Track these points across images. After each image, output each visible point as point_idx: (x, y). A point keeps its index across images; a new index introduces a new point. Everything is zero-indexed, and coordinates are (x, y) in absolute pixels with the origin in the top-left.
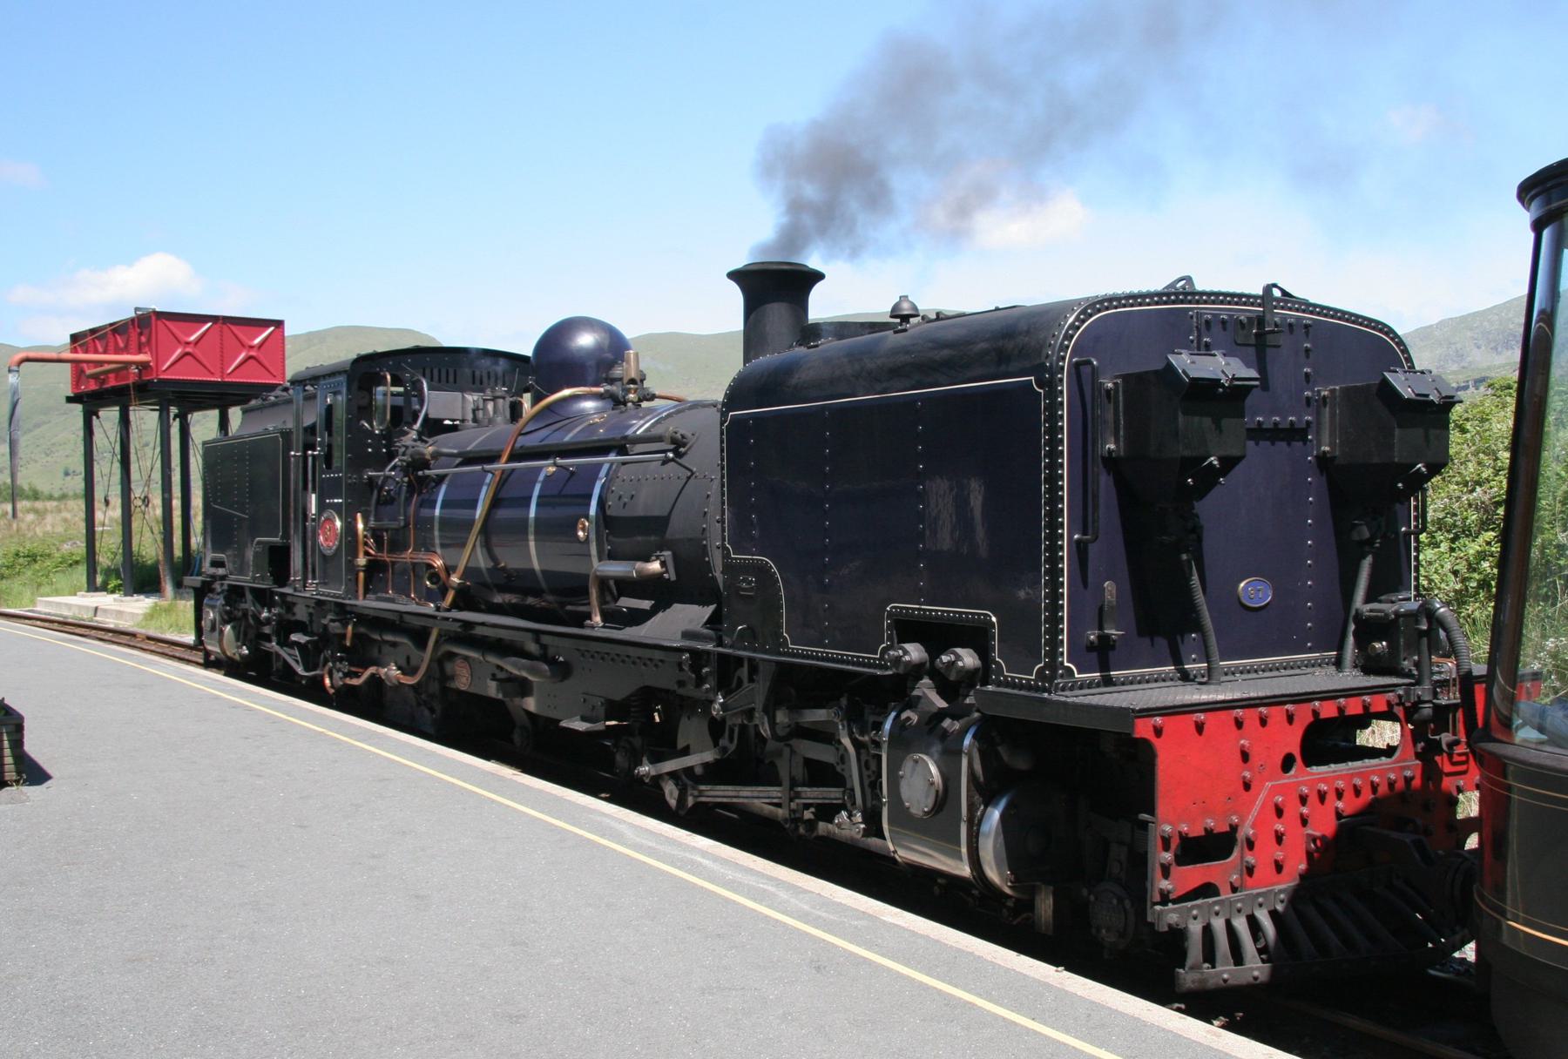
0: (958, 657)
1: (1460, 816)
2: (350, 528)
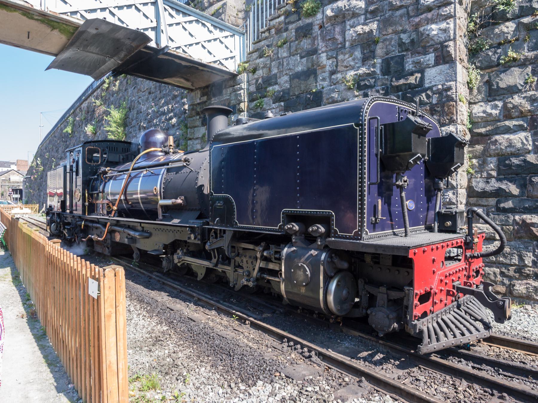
0: (318, 228)
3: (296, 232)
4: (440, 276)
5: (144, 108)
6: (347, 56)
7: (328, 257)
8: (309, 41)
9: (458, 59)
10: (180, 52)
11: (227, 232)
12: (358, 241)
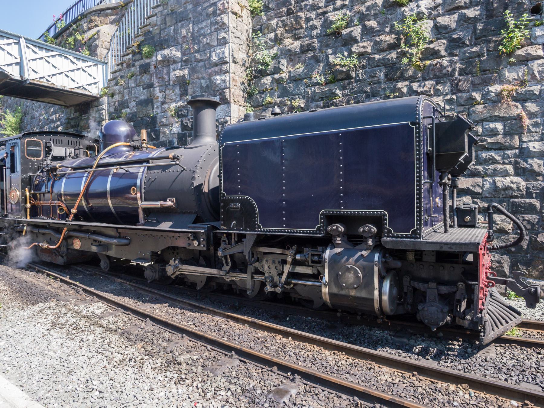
1: (472, 260)
2: (24, 195)
3: (339, 234)
5: (37, 114)
6: (171, 92)
8: (148, 77)
9: (232, 101)
10: (44, 83)
11: (248, 237)
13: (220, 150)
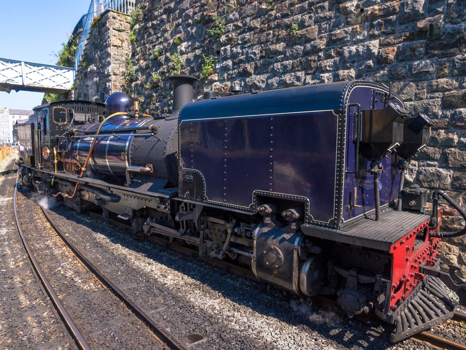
2: (52, 153)
3: (268, 215)
4: (411, 263)
7: (302, 242)
12: (334, 230)
13: (179, 127)
